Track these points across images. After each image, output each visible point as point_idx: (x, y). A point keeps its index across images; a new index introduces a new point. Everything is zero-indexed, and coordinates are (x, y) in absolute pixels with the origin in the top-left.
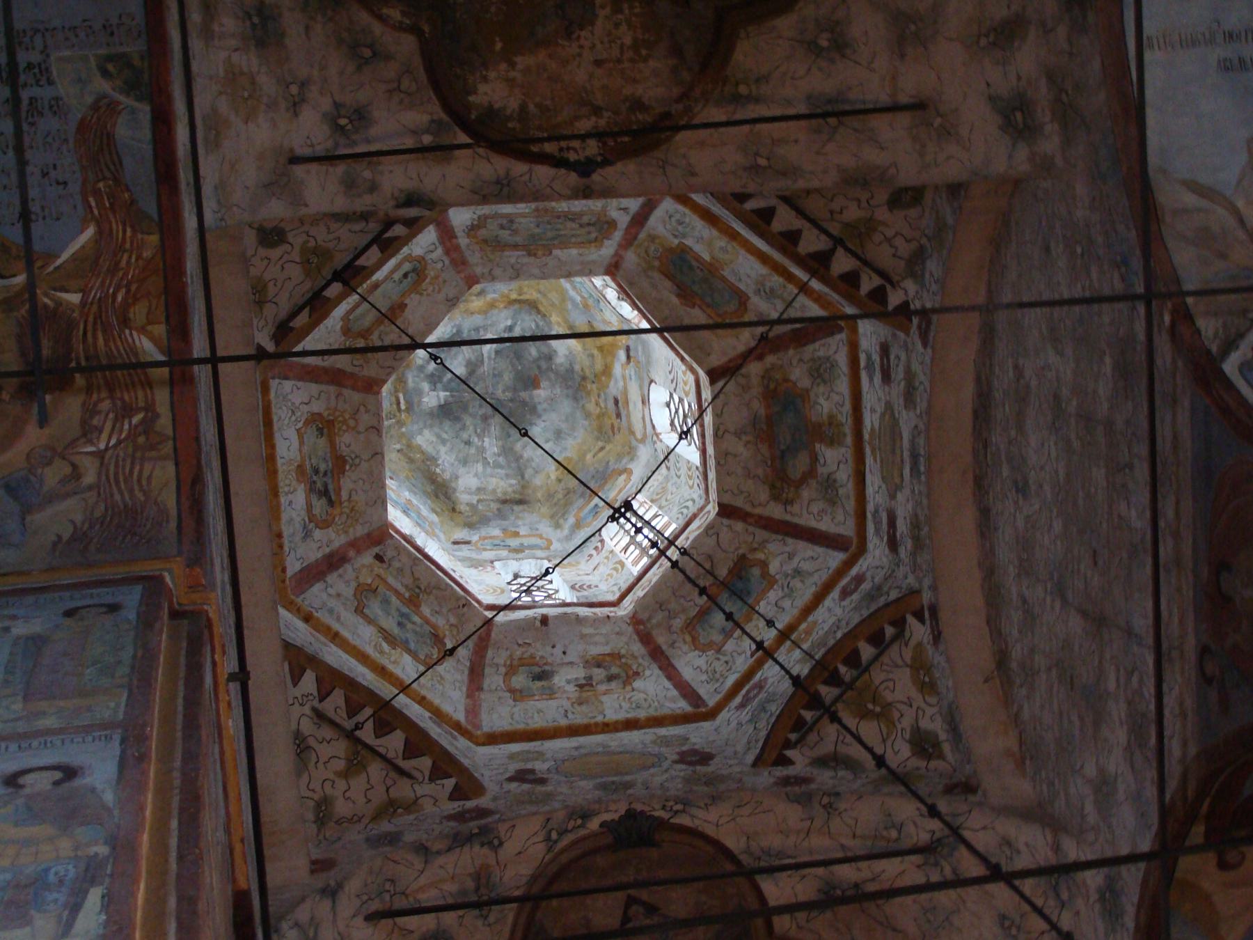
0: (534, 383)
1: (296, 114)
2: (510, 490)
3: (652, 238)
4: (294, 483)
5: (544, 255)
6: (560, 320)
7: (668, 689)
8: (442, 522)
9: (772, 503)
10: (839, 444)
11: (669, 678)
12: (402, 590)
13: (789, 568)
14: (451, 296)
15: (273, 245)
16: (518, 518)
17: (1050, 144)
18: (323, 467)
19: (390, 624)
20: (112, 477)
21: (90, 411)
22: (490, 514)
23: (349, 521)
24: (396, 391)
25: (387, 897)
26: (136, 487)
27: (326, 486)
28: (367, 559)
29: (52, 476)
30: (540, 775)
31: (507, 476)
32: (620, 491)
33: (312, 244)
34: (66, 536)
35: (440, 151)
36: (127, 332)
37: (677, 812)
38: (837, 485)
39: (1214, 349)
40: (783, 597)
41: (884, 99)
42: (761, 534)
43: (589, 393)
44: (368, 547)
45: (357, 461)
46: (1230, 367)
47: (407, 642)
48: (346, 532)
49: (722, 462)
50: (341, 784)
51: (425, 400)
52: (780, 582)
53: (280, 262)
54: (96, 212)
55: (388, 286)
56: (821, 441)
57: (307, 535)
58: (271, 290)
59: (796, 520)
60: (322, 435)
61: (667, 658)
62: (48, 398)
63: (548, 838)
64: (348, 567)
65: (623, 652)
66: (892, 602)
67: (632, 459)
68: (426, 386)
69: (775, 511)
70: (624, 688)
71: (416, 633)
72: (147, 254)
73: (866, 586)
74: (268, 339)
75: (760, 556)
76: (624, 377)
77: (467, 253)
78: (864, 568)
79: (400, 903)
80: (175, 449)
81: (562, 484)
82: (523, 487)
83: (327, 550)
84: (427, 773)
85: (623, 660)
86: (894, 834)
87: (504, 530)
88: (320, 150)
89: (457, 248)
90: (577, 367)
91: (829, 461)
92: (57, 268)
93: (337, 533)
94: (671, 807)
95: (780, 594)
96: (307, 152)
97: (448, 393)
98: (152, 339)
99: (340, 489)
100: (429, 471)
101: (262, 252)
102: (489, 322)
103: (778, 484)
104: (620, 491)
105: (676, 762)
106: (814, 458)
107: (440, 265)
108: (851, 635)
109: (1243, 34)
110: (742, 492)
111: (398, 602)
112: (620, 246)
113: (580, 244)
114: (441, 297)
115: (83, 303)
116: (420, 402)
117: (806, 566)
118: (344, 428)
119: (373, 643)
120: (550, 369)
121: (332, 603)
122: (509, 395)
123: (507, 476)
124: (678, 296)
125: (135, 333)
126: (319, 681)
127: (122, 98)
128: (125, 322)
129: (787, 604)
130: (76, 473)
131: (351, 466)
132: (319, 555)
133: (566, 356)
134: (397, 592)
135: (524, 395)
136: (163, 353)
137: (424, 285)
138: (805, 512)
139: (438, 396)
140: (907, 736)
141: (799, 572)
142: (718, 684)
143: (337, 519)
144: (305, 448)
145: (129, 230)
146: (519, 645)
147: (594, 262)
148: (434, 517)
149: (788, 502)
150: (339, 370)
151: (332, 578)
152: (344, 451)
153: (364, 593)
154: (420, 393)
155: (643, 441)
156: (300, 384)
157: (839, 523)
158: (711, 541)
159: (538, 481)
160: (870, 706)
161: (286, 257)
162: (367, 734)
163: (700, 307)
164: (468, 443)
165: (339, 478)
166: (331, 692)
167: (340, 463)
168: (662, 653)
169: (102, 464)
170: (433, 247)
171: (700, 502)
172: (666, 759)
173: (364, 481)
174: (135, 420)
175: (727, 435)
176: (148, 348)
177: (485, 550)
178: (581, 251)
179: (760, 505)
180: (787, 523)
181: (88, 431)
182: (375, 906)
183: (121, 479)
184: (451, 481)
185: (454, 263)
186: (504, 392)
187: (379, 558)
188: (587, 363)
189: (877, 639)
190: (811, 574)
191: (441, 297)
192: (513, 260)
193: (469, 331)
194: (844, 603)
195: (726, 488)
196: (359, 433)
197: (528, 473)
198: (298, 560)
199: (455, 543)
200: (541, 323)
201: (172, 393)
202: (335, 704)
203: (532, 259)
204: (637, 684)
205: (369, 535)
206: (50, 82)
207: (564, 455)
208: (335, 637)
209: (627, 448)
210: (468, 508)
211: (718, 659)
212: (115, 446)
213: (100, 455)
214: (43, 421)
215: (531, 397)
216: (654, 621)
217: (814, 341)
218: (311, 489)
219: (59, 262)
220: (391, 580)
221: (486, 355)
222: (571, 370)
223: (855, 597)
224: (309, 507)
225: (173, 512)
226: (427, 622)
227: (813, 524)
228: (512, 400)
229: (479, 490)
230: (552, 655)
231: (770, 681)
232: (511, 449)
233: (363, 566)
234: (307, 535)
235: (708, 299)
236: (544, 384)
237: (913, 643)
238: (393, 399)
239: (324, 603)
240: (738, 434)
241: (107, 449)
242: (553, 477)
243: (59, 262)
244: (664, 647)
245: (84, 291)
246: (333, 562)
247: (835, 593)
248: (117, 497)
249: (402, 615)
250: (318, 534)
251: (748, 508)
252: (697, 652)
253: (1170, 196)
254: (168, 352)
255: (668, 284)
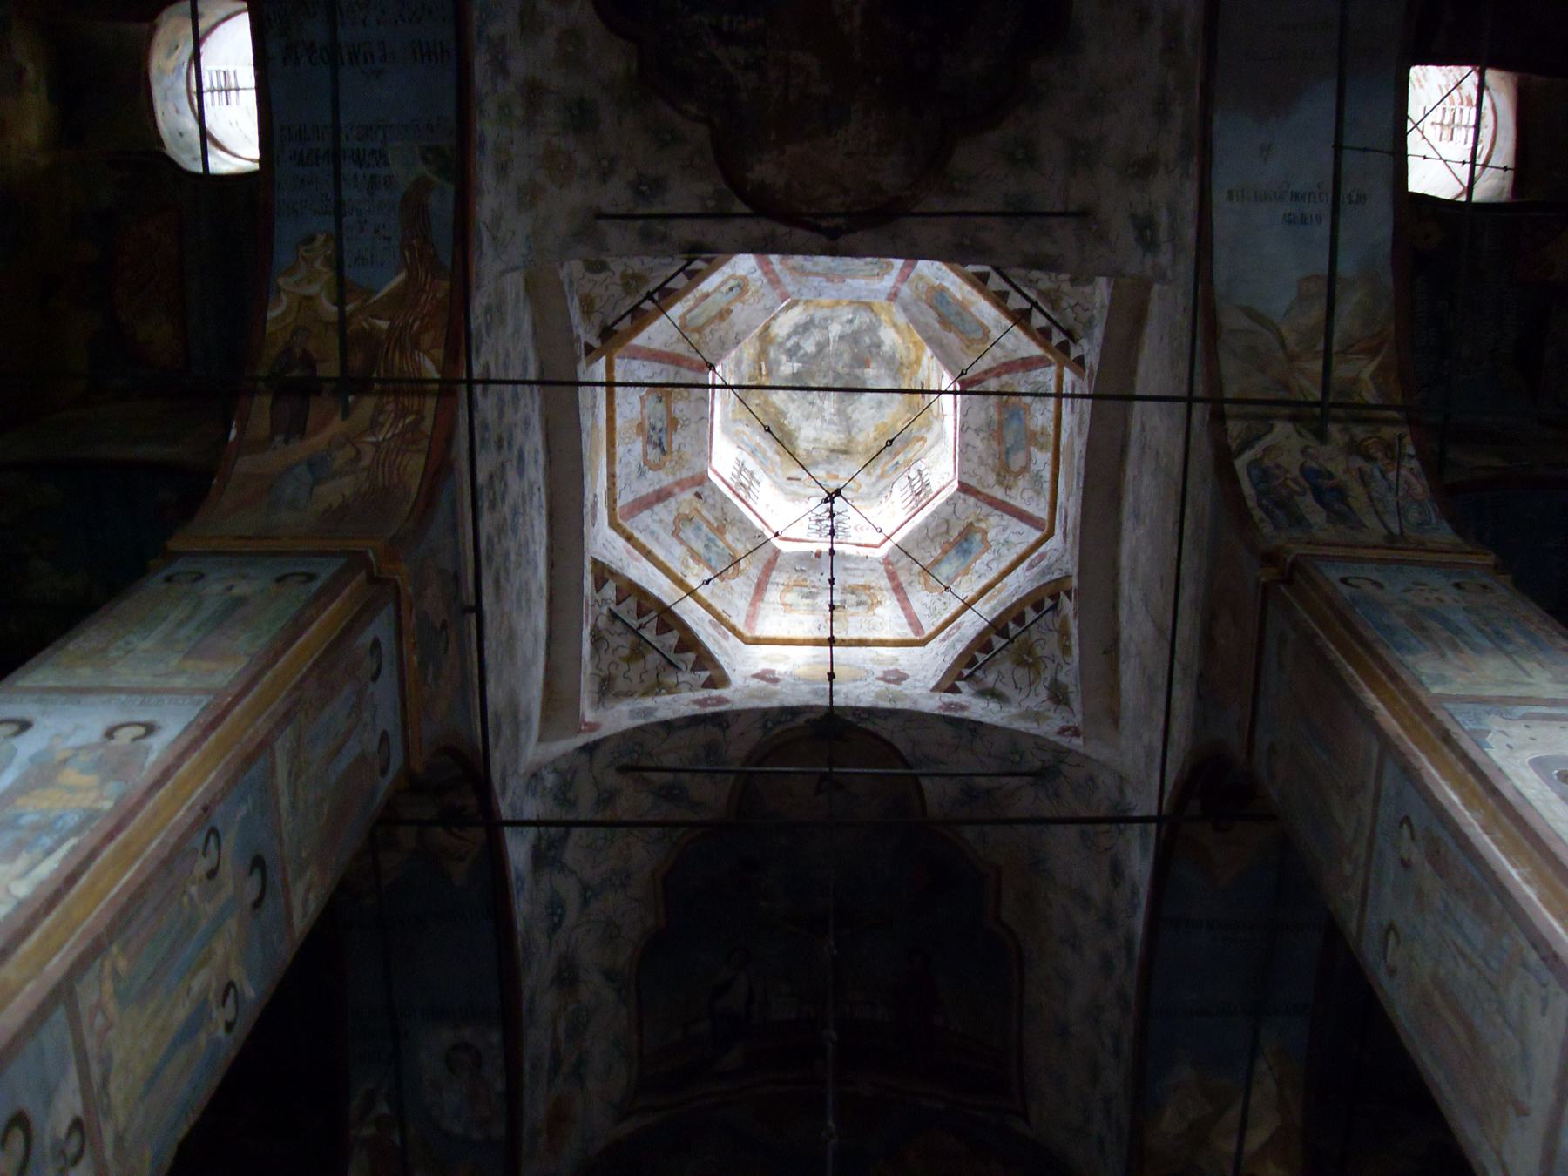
0: (866, 364)
1: (605, 182)
2: (838, 442)
3: (921, 278)
4: (634, 437)
5: (839, 282)
6: (887, 319)
7: (900, 617)
8: (782, 462)
9: (997, 487)
10: (1046, 449)
11: (903, 609)
12: (712, 520)
13: (1001, 538)
14: (768, 306)
15: (600, 271)
16: (840, 464)
17: (1164, 259)
18: (659, 425)
19: (698, 546)
20: (381, 462)
21: (379, 410)
22: (820, 459)
23: (678, 466)
24: (760, 360)
25: (636, 756)
26: (395, 472)
27: (660, 439)
28: (688, 495)
29: (341, 458)
30: (777, 676)
31: (838, 431)
32: (915, 454)
33: (630, 271)
34: (335, 505)
35: (722, 216)
36: (416, 352)
37: (862, 719)
38: (1043, 480)
39: (1234, 446)
40: (993, 560)
41: (1059, 208)
42: (986, 509)
43: (904, 376)
44: (691, 486)
45: (688, 422)
46: (1240, 464)
47: (709, 560)
48: (674, 474)
49: (964, 451)
50: (624, 667)
51: (782, 368)
52: (993, 548)
53: (605, 284)
54: (409, 261)
55: (718, 296)
56: (1035, 445)
57: (641, 474)
58: (598, 304)
59: (1012, 502)
60: (661, 401)
61: (905, 593)
62: (351, 398)
63: (765, 726)
64: (672, 500)
65: (873, 584)
66: (1053, 581)
67: (928, 431)
68: (784, 358)
69: (998, 493)
70: (868, 612)
71: (718, 554)
72: (440, 295)
73: (1044, 563)
74: (595, 338)
75: (983, 525)
76: (929, 368)
77: (781, 276)
78: (1049, 548)
79: (645, 762)
80: (430, 447)
81: (878, 442)
82: (849, 441)
83: (657, 487)
84: (690, 666)
85: (872, 591)
86: (1017, 758)
87: (828, 473)
88: (623, 210)
89: (773, 271)
90: (898, 356)
91: (1038, 462)
92: (375, 302)
93: (667, 475)
94: (859, 715)
95: (992, 557)
96: (612, 210)
97: (800, 365)
98: (433, 361)
99: (672, 442)
100: (778, 422)
101: (589, 276)
102: (835, 315)
103: (1002, 473)
104: (915, 454)
105: (879, 679)
106: (1029, 458)
107: (759, 283)
108: (1021, 601)
109: (1307, 196)
110: (976, 475)
111: (708, 529)
112: (897, 280)
113: (865, 277)
114: (760, 306)
115: (390, 328)
116: (778, 370)
117: (1013, 538)
118: (679, 397)
119: (682, 559)
120: (878, 354)
121: (654, 527)
122: (846, 370)
123: (838, 431)
124: (939, 322)
125: (421, 354)
126: (618, 589)
127: (435, 178)
128: (416, 345)
129: (994, 565)
130: (358, 455)
131: (682, 426)
132: (651, 490)
133: (890, 346)
134: (708, 522)
135: (858, 372)
136: (438, 370)
137: (746, 297)
138: (1019, 497)
139: (793, 367)
140: (1047, 684)
141: (1007, 542)
142: (935, 619)
143: (668, 463)
144: (646, 412)
145: (429, 276)
146: (797, 570)
147: (878, 291)
148: (777, 458)
149: (1008, 488)
150: (679, 355)
151: (659, 508)
152: (678, 414)
153: (682, 520)
154: (779, 363)
155: (937, 418)
156: (646, 363)
157: (1040, 510)
158: (950, 509)
159: (861, 437)
160: (1025, 657)
161: (608, 281)
162: (650, 634)
163: (955, 332)
164: (812, 403)
165: (671, 435)
166: (627, 598)
167: (673, 423)
168: (902, 588)
169: (377, 451)
170: (753, 270)
171: (950, 478)
172: (873, 674)
173: (691, 438)
174: (408, 420)
175: (969, 431)
176: (430, 370)
177: (809, 487)
178: (868, 281)
179: (988, 486)
180: (1004, 502)
181: (374, 425)
182: (625, 761)
183: (387, 465)
184: (795, 431)
185: (771, 282)
186: (843, 367)
187: (698, 495)
188: (904, 353)
189: (1038, 606)
190: (1015, 545)
191: (760, 306)
192: (816, 284)
193: (820, 320)
194: (1027, 574)
195: (966, 470)
196: (690, 401)
197: (855, 430)
198: (633, 492)
199: (790, 479)
200: (874, 320)
201: (438, 402)
202: (627, 611)
203: (830, 284)
204: (878, 610)
205: (693, 478)
206: (387, 164)
207: (881, 420)
208: (648, 554)
209: (926, 421)
210: (804, 453)
211: (940, 600)
212: (390, 439)
213: (377, 445)
214: (345, 416)
215: (863, 373)
216: (900, 564)
217: (1036, 369)
218: (649, 440)
219: (379, 296)
220: (705, 513)
221: (831, 339)
222: (892, 358)
223: (1036, 570)
224: (645, 455)
225: (414, 495)
226: (729, 546)
227: (1024, 507)
228: (848, 374)
229: (816, 440)
230: (820, 580)
231: (965, 624)
232: (844, 411)
233: (685, 500)
234: (641, 474)
235: (961, 328)
236: (873, 365)
237: (1062, 614)
238: (757, 367)
239: (648, 527)
240: (977, 431)
241: (384, 439)
242: (872, 436)
243: (379, 296)
244: (904, 585)
245: (392, 320)
246: (662, 496)
247: (1025, 565)
248: (380, 477)
249: (710, 540)
250: (650, 474)
251: (980, 488)
252: (926, 592)
253: (1232, 320)
254: (441, 371)
255: (932, 313)
